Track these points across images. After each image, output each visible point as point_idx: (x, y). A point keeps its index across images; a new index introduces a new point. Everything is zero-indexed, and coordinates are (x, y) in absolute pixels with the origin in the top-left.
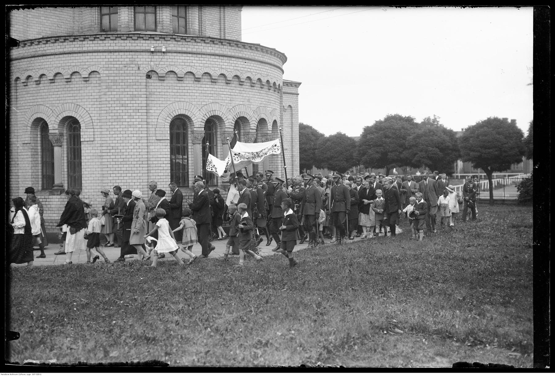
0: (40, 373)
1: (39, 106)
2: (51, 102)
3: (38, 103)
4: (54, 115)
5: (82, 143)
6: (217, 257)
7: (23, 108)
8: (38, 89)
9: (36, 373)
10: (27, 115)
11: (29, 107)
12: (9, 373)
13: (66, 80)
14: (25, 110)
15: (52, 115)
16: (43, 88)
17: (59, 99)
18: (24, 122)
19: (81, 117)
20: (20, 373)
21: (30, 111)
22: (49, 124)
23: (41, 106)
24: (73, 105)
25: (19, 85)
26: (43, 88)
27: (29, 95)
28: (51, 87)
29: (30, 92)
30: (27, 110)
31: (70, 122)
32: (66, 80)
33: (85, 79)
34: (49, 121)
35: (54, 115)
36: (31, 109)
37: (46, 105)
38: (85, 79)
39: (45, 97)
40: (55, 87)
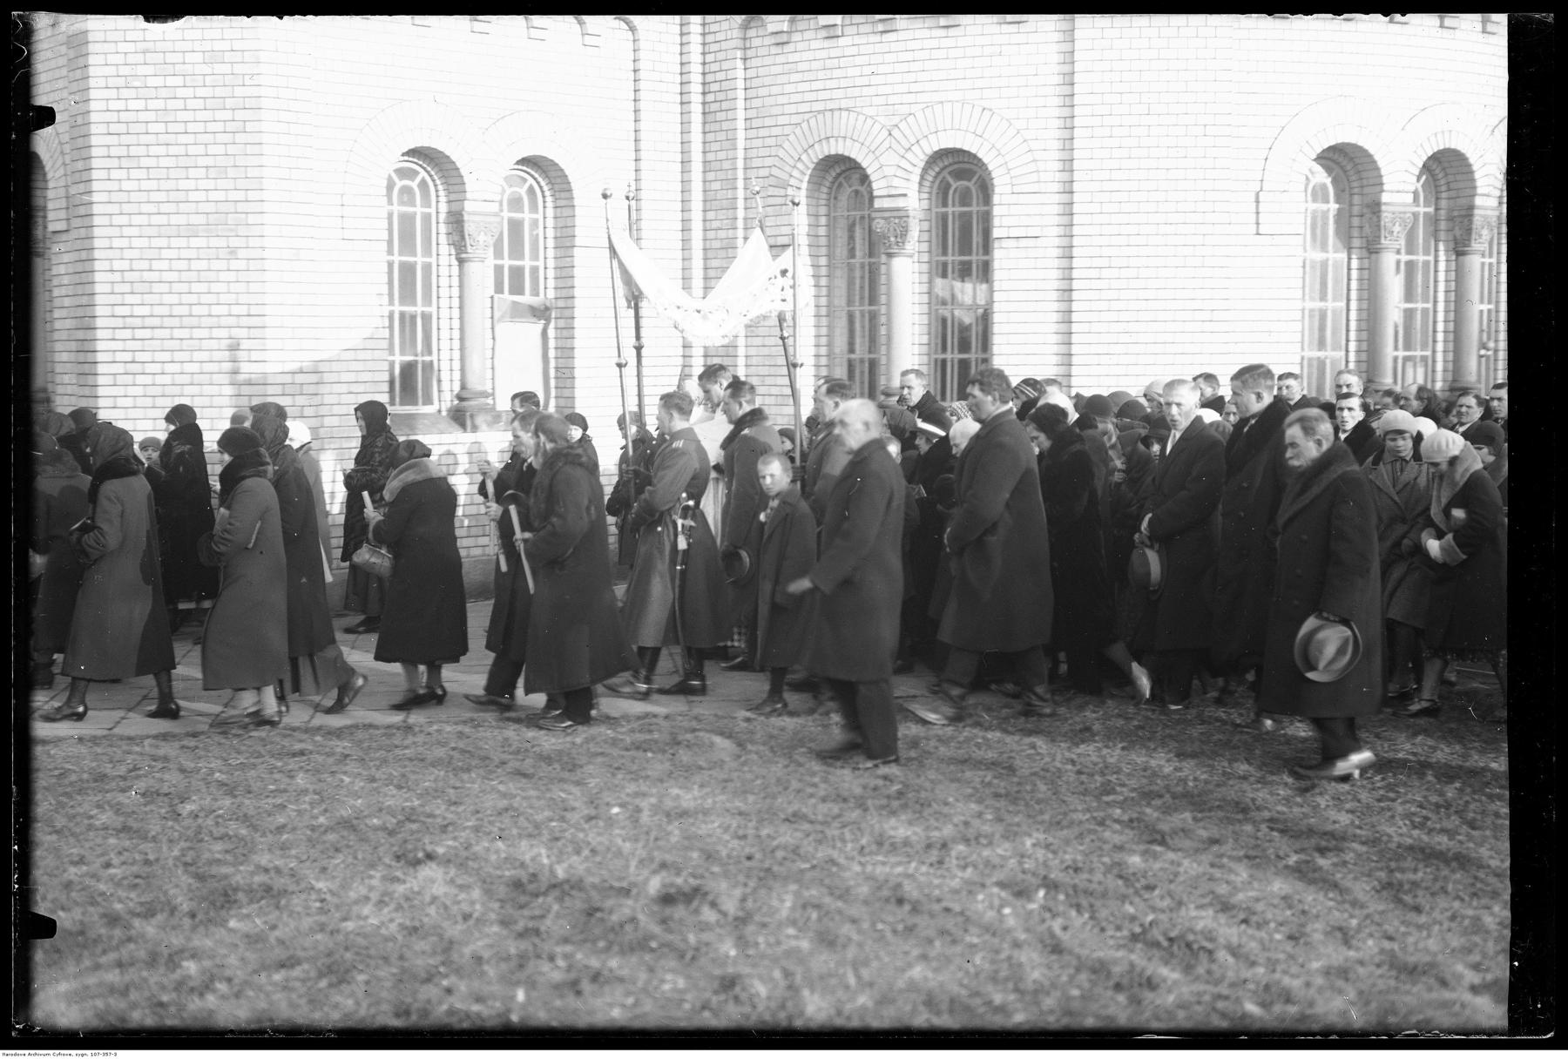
0: (113, 1052)
1: (837, 114)
2: (881, 100)
3: (830, 105)
4: (895, 145)
5: (996, 244)
6: (345, 656)
7: (768, 122)
8: (834, 53)
9: (101, 1052)
10: (786, 145)
11: (795, 119)
12: (27, 1052)
13: (773, 40)
14: (775, 131)
15: (886, 145)
16: (854, 50)
17: (914, 88)
18: (775, 171)
19: (994, 152)
20: (57, 1052)
21: (798, 131)
22: (872, 178)
23: (844, 114)
24: (968, 108)
25: (756, 42)
26: (854, 50)
27: (795, 77)
28: (885, 47)
29: (801, 67)
30: (787, 130)
31: (942, 169)
32: (773, 40)
33: (780, 39)
34: (876, 165)
35: (895, 145)
36: (805, 125)
37: (866, 111)
38: (780, 39)
39: (859, 81)
40: (901, 46)
